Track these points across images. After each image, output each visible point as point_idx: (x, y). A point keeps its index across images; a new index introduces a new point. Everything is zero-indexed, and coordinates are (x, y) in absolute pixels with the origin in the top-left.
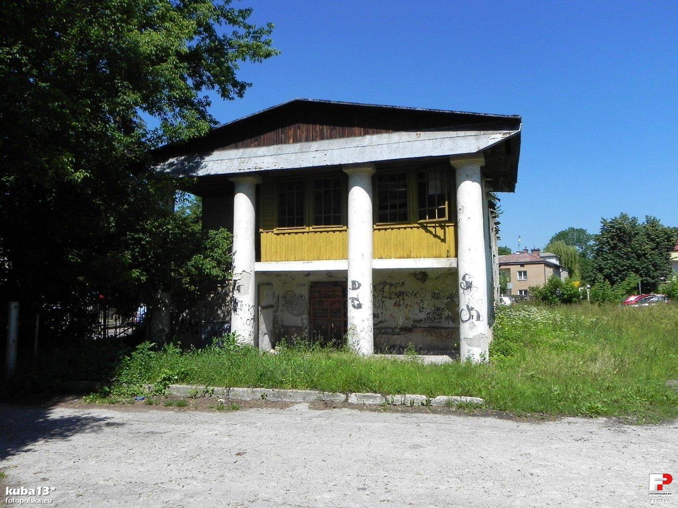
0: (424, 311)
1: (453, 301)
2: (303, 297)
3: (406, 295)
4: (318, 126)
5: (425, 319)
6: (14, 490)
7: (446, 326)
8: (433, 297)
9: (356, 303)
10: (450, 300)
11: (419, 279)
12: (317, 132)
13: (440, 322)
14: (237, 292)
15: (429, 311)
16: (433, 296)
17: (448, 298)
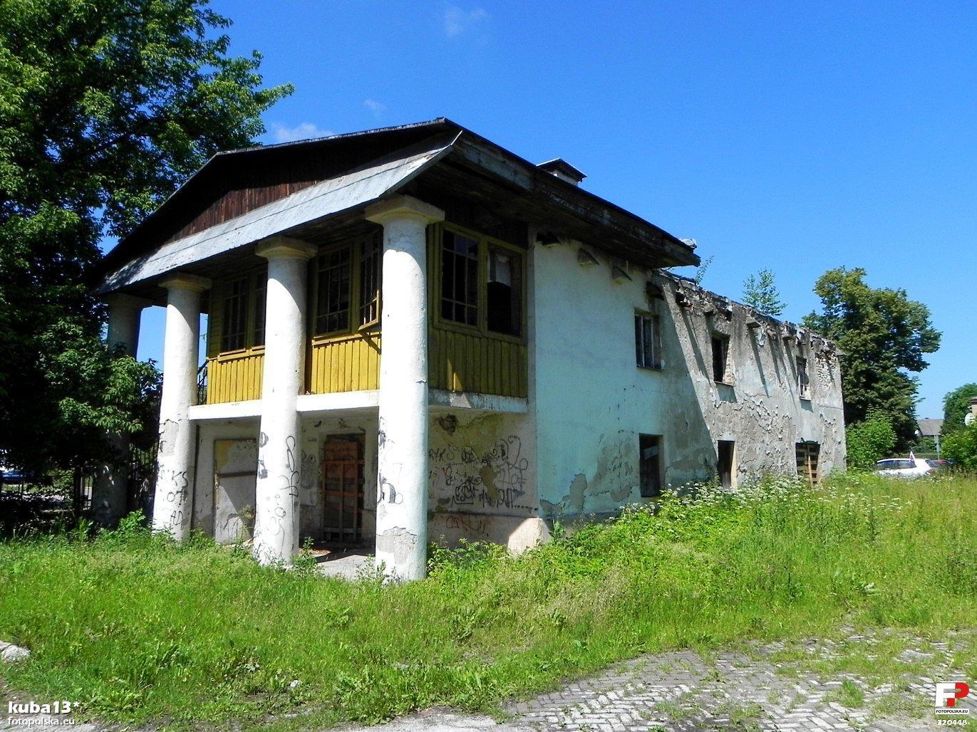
0: (452, 483)
1: (490, 466)
2: (313, 459)
6: (21, 706)
7: (480, 511)
8: (464, 460)
11: (445, 428)
15: (459, 483)
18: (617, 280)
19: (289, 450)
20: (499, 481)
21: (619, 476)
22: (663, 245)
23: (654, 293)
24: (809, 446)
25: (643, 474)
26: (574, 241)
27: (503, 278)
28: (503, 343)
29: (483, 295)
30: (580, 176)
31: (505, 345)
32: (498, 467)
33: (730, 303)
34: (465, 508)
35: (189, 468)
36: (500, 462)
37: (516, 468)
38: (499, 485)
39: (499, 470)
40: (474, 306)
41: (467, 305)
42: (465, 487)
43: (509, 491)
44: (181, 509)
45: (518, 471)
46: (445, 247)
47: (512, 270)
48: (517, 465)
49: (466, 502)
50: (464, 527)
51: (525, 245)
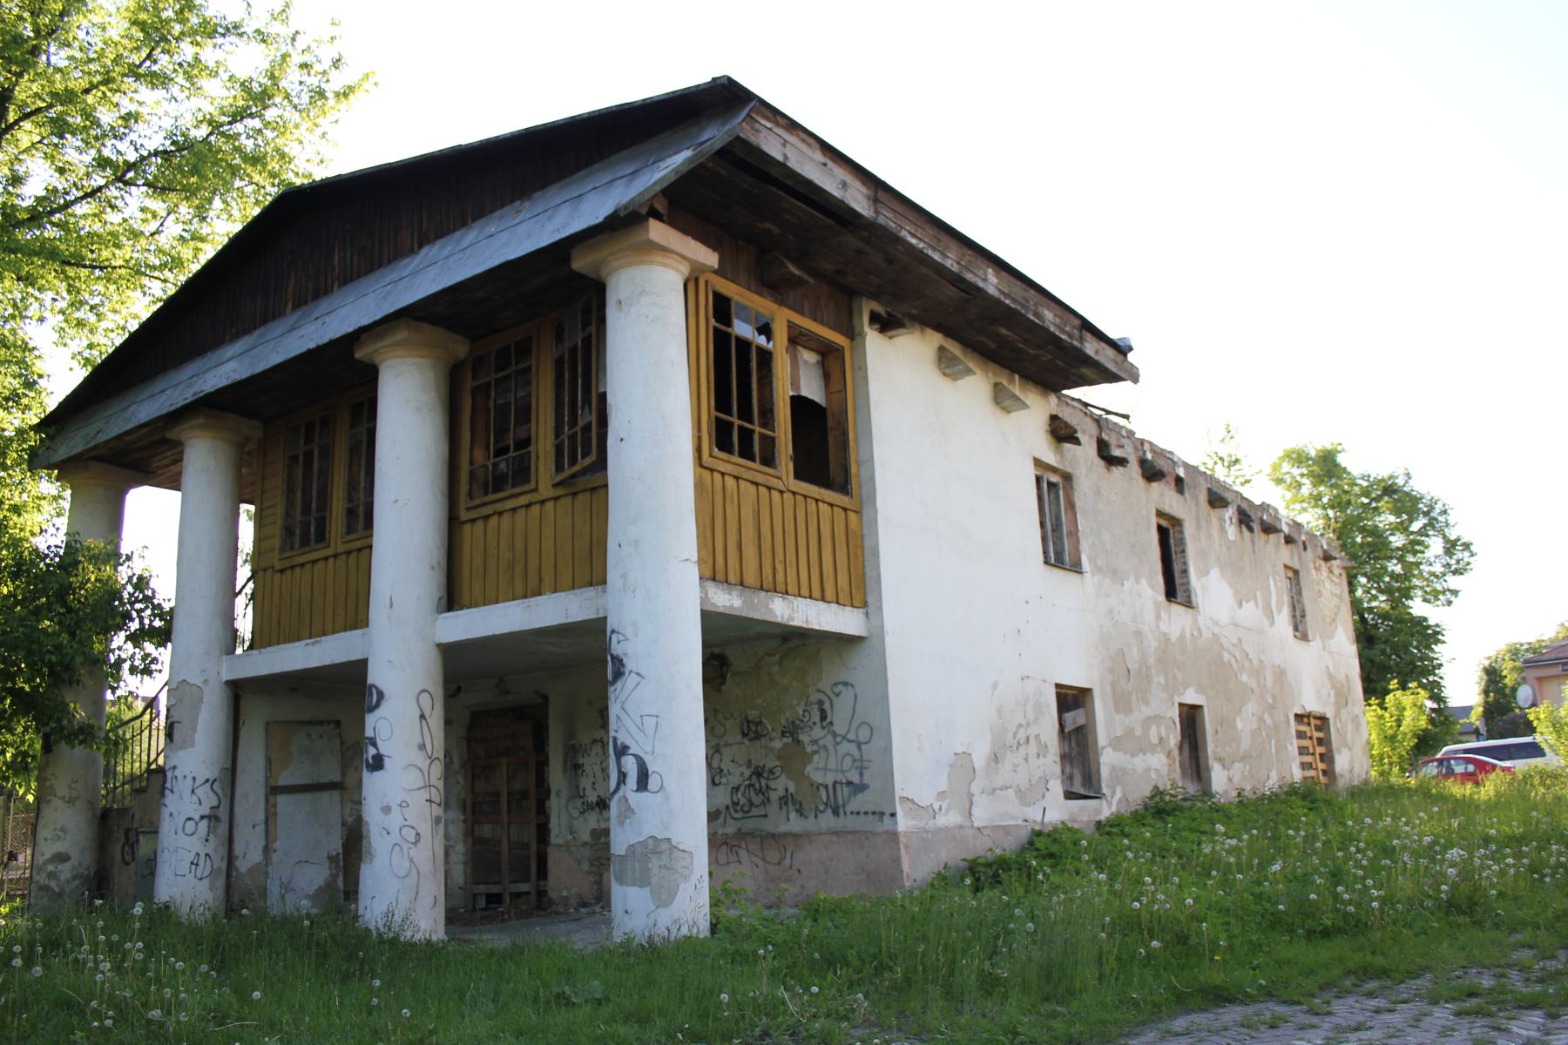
0: (724, 780)
5: (727, 807)
8: (744, 735)
9: (372, 751)
10: (789, 740)
13: (766, 816)
16: (746, 731)
17: (783, 734)
19: (422, 716)
21: (1026, 759)
23: (1061, 433)
24: (1313, 722)
27: (812, 390)
28: (820, 504)
29: (783, 413)
32: (815, 742)
34: (749, 825)
35: (224, 770)
36: (818, 732)
37: (849, 741)
38: (818, 777)
39: (815, 748)
40: (770, 433)
42: (749, 786)
43: (838, 786)
44: (210, 848)
45: (853, 748)
46: (716, 321)
47: (827, 377)
48: (851, 736)
49: (753, 813)
50: (752, 862)
51: (853, 334)
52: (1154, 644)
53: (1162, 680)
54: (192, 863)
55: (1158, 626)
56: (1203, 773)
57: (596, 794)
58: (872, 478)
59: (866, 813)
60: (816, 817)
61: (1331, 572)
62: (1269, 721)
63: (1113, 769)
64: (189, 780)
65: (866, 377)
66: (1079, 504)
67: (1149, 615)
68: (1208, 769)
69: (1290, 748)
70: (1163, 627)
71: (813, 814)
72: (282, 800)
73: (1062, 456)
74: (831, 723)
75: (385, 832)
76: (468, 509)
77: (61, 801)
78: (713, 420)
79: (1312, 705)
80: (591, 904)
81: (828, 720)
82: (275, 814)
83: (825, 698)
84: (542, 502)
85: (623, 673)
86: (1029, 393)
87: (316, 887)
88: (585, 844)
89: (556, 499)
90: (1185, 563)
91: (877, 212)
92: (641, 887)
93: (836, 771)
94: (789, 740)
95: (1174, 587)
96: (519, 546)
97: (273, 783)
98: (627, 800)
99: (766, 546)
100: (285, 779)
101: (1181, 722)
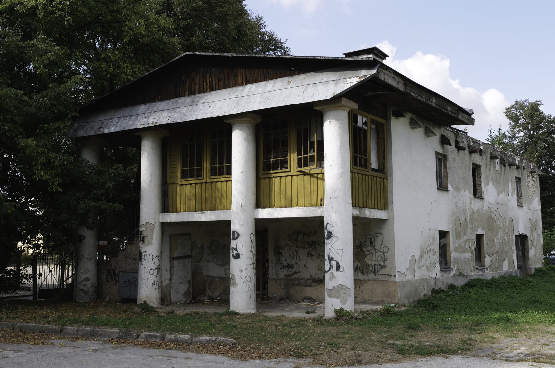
3: (318, 244)
4: (239, 70)
9: (235, 252)
12: (208, 84)
14: (142, 242)
18: (428, 135)
19: (251, 242)
20: (369, 260)
21: (430, 257)
22: (458, 114)
23: (444, 141)
25: (441, 255)
26: (408, 113)
28: (377, 178)
30: (385, 56)
31: (360, 176)
32: (368, 251)
33: (482, 144)
36: (369, 248)
37: (380, 252)
38: (369, 262)
39: (368, 253)
41: (363, 157)
43: (376, 266)
45: (381, 254)
48: (381, 250)
51: (388, 120)
52: (469, 213)
53: (471, 226)
54: (153, 284)
55: (471, 207)
56: (482, 259)
57: (287, 262)
58: (392, 168)
59: (385, 275)
60: (368, 275)
61: (533, 177)
62: (506, 238)
63: (454, 259)
64: (151, 256)
65: (391, 134)
66: (448, 165)
67: (468, 203)
68: (484, 257)
69: (513, 249)
70: (472, 207)
71: (367, 274)
72: (175, 262)
73: (444, 149)
74: (374, 245)
75: (241, 278)
76: (263, 174)
77: (86, 260)
78: (353, 156)
79: (522, 231)
80: (285, 299)
81: (373, 245)
82: (173, 266)
83: (372, 237)
84: (292, 176)
85: (332, 236)
86: (436, 129)
87: (184, 291)
88: (282, 279)
89: (298, 175)
90: (481, 182)
91: (406, 89)
92: (337, 298)
93: (376, 261)
94: (359, 250)
95: (477, 193)
96: (283, 189)
97: (172, 256)
98: (333, 274)
99: (365, 194)
100: (176, 255)
101: (476, 241)
